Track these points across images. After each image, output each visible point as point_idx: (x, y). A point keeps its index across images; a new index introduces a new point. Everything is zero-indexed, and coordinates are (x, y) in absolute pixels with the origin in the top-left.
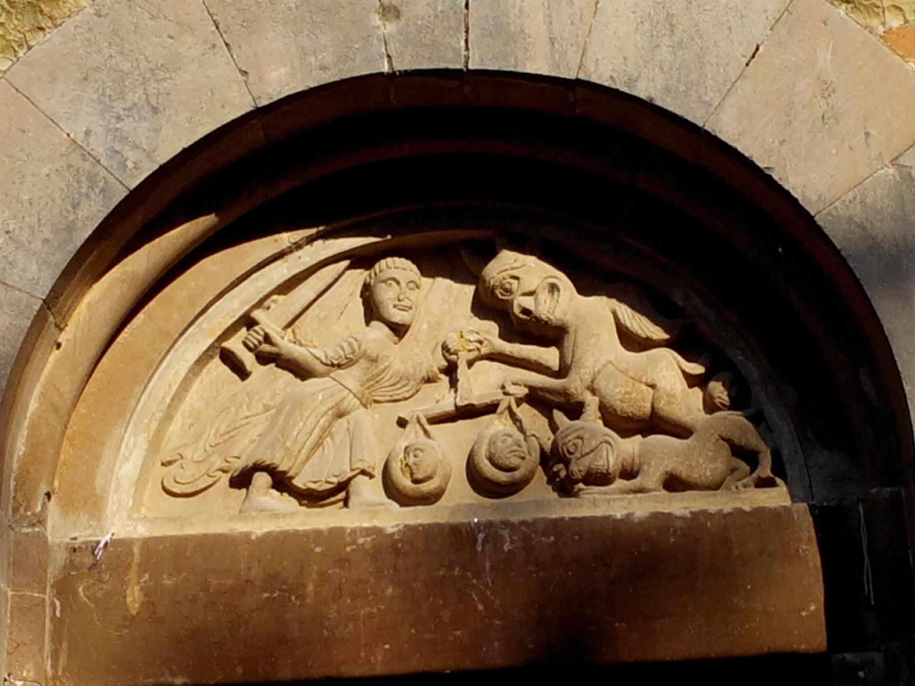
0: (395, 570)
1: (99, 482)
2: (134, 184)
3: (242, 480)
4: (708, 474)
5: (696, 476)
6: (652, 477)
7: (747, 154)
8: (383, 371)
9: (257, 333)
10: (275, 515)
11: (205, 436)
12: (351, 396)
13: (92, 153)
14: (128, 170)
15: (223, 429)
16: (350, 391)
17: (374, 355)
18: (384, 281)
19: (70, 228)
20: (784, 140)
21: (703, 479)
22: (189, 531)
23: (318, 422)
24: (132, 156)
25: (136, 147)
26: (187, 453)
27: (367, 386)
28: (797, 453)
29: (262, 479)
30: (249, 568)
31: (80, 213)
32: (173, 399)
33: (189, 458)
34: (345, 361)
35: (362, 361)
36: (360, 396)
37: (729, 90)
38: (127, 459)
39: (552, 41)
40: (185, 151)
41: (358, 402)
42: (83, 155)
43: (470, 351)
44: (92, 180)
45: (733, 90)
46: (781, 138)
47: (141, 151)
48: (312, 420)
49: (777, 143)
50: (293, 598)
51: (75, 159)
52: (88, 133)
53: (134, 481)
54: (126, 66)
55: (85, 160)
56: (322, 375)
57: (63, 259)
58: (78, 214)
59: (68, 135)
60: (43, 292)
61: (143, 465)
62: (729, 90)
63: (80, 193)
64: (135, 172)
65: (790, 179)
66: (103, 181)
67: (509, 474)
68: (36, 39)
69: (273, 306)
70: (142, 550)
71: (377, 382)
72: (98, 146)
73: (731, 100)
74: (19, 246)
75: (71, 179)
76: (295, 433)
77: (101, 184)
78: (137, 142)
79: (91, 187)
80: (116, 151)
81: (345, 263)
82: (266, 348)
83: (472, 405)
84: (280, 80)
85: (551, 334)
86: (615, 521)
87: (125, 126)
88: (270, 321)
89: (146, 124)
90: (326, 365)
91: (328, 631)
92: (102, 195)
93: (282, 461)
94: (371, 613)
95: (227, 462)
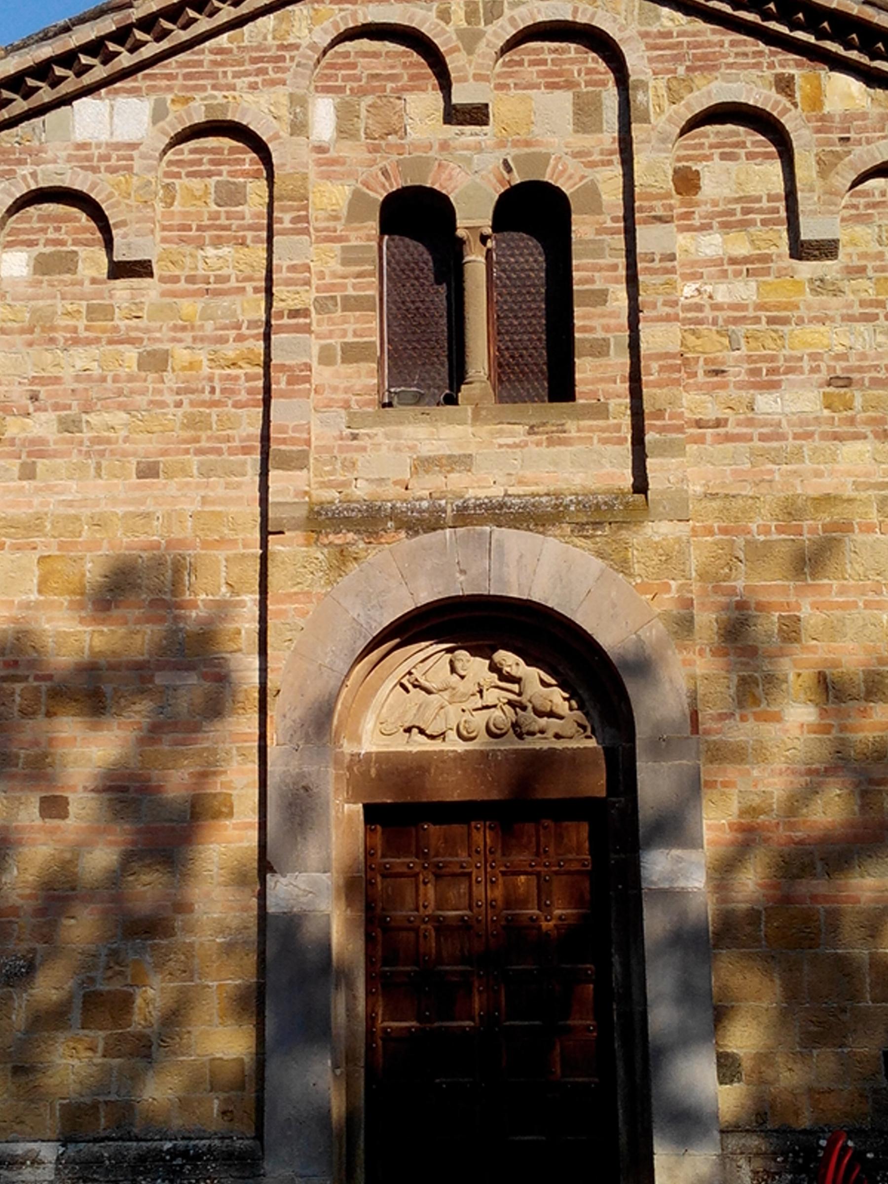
3: (408, 730)
6: (550, 734)
10: (420, 744)
19: (353, 650)
24: (374, 625)
29: (415, 731)
51: (354, 625)
88: (417, 674)
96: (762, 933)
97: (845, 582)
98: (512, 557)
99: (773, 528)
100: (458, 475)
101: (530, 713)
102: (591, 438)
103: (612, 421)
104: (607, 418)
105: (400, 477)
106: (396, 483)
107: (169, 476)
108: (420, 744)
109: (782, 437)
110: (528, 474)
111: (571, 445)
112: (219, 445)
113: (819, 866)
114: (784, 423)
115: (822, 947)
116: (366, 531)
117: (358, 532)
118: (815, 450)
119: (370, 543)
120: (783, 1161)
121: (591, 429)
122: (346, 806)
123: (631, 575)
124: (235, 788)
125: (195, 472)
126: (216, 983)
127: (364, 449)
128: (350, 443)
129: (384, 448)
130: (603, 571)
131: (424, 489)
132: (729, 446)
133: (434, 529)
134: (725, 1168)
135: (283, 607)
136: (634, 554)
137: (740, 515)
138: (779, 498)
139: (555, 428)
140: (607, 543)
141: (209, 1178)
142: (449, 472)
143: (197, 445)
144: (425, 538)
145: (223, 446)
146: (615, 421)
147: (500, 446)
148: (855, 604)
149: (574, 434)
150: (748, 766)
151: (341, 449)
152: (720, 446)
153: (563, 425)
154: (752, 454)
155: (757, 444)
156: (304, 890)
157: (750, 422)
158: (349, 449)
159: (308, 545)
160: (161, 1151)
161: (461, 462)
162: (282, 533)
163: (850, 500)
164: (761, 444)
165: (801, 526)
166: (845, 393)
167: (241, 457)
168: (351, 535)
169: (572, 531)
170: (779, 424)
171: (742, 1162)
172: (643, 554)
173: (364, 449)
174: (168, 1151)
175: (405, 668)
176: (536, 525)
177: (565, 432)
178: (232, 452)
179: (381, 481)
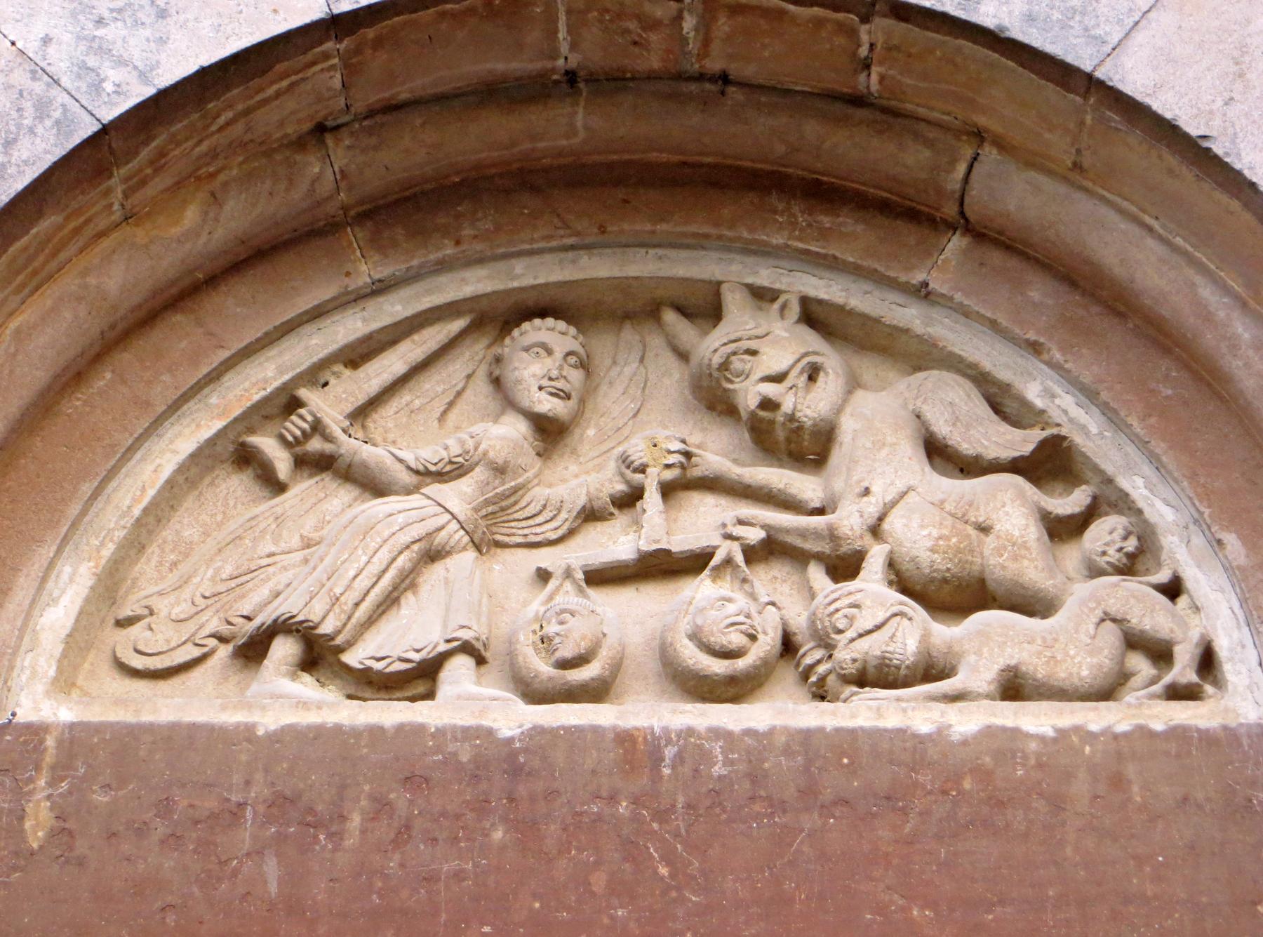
0: (511, 800)
2: (109, 115)
3: (253, 650)
4: (1085, 673)
5: (1063, 675)
6: (978, 673)
7: (1168, 115)
8: (515, 490)
9: (301, 417)
11: (196, 580)
12: (454, 525)
13: (48, 69)
14: (104, 95)
15: (228, 570)
16: (454, 517)
17: (500, 461)
18: (527, 349)
20: (1232, 99)
21: (1076, 681)
22: (146, 718)
23: (394, 559)
24: (113, 75)
27: (484, 512)
28: (1243, 647)
29: (284, 650)
30: (248, 783)
31: (16, 154)
32: (146, 511)
33: (163, 613)
34: (448, 468)
35: (478, 469)
36: (470, 527)
37: (1137, 23)
38: (55, 601)
40: (203, 72)
41: (466, 539)
42: (33, 72)
43: (668, 466)
44: (42, 108)
45: (1143, 22)
46: (1227, 95)
47: (129, 69)
48: (384, 556)
49: (1219, 103)
50: (322, 837)
51: (20, 77)
52: (47, 40)
53: (63, 636)
55: (34, 79)
56: (408, 491)
58: (11, 155)
59: (13, 44)
61: (80, 613)
62: (1137, 23)
63: (19, 126)
64: (114, 98)
65: (1243, 154)
66: (60, 110)
67: (726, 662)
69: (333, 381)
70: (60, 743)
71: (503, 509)
72: (60, 60)
73: (1139, 37)
75: (8, 105)
76: (352, 573)
77: (57, 114)
78: (126, 56)
79: (40, 118)
80: (88, 68)
81: (458, 325)
82: (315, 445)
83: (667, 552)
85: (810, 447)
86: (915, 736)
87: (112, 32)
88: (329, 405)
89: (147, 32)
90: (417, 472)
91: (381, 897)
92: (54, 131)
93: (324, 618)
94: (463, 871)
95: (229, 623)
101: (872, 582)
108: (304, 705)
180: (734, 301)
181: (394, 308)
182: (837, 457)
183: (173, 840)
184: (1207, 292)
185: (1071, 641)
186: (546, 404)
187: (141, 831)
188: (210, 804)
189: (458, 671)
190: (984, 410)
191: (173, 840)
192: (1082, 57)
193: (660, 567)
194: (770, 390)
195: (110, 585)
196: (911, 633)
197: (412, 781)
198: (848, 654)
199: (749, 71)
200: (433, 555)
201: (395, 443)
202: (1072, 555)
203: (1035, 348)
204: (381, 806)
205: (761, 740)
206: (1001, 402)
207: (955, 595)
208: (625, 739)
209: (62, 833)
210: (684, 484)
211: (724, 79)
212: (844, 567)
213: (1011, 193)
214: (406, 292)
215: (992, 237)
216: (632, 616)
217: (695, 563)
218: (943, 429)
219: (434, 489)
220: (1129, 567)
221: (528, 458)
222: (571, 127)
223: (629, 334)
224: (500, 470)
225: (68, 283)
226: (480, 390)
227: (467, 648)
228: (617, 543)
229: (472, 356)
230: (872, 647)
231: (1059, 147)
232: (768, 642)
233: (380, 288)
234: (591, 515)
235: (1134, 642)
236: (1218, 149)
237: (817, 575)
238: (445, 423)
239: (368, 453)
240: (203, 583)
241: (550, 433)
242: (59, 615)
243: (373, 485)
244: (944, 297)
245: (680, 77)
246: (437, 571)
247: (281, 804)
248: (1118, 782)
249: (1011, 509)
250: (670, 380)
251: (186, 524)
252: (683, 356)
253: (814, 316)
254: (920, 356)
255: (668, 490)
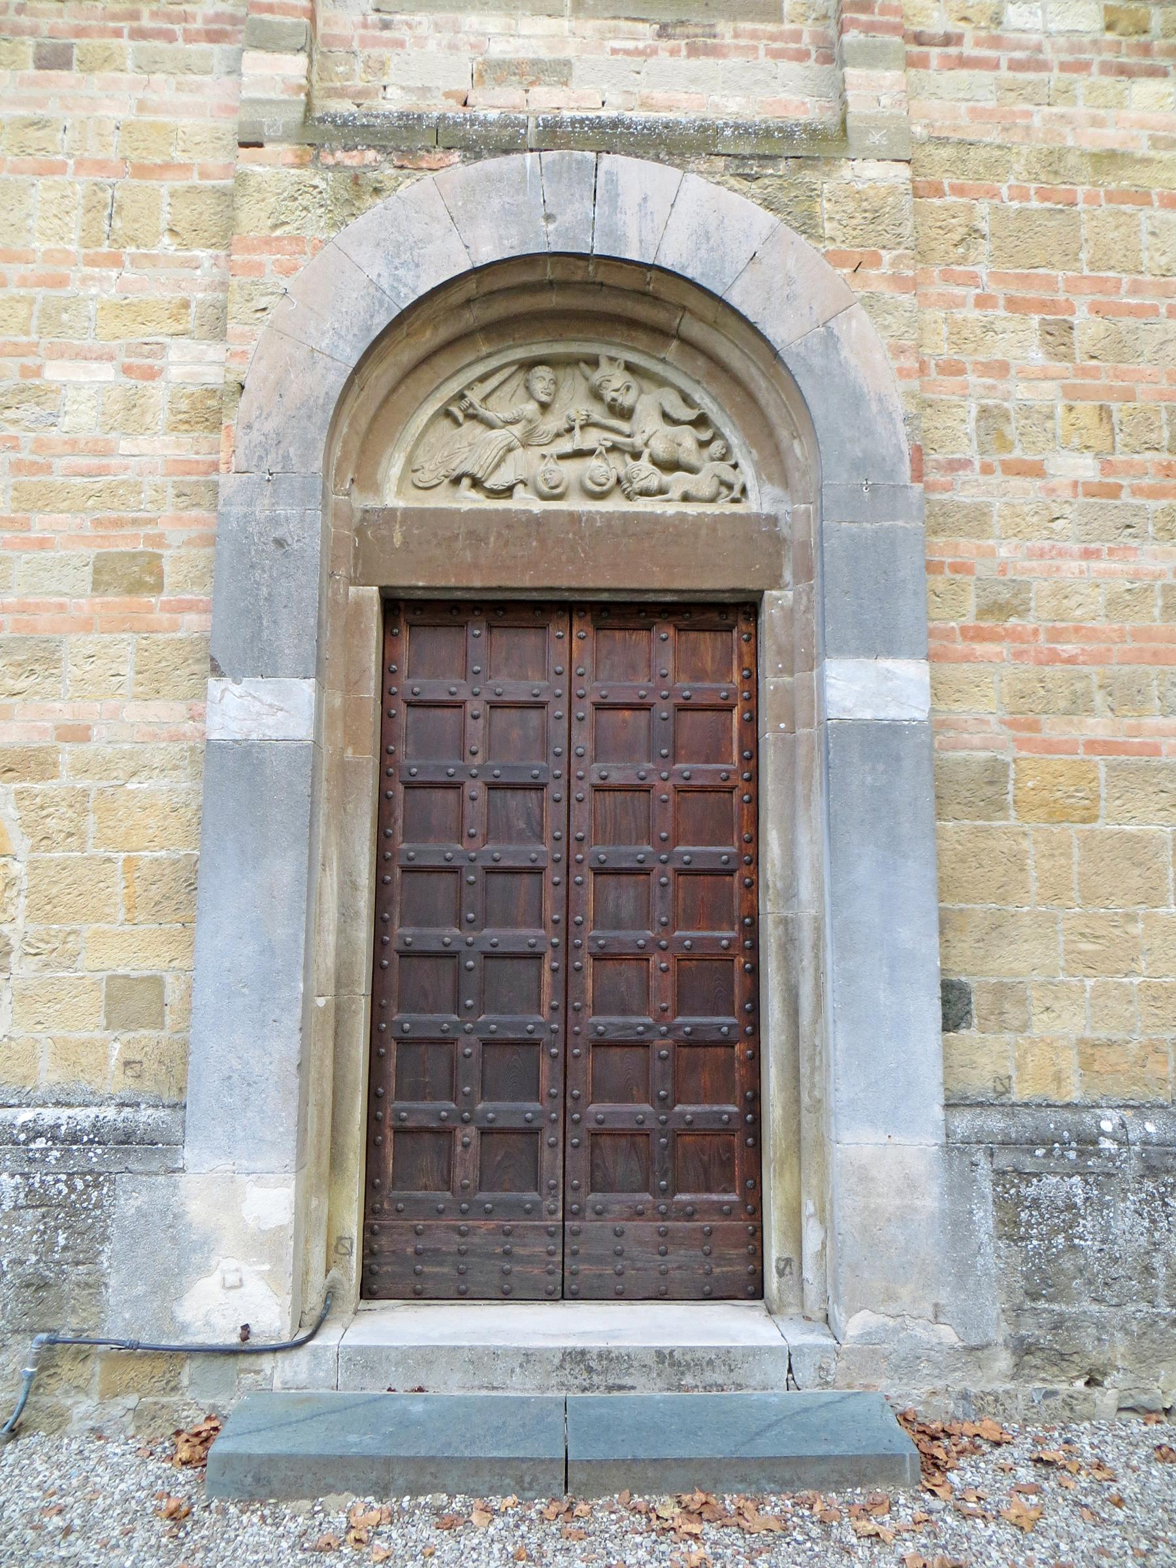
1: (379, 476)
2: (404, 306)
3: (456, 481)
6: (675, 493)
10: (474, 501)
19: (369, 329)
24: (404, 291)
25: (405, 285)
26: (426, 466)
29: (466, 482)
39: (641, 241)
51: (372, 290)
54: (401, 239)
57: (364, 346)
60: (353, 363)
68: (351, 221)
72: (385, 283)
74: (340, 337)
81: (514, 368)
82: (471, 411)
84: (488, 253)
85: (626, 414)
87: (401, 272)
88: (474, 397)
96: (1010, 798)
97: (1140, 277)
98: (629, 200)
99: (1032, 192)
100: (546, 89)
101: (644, 461)
102: (755, 48)
103: (787, 26)
104: (781, 20)
105: (455, 88)
106: (448, 95)
107: (89, 68)
108: (474, 501)
109: (1042, 66)
110: (659, 95)
111: (724, 56)
112: (170, 26)
113: (1099, 698)
114: (1047, 47)
115: (1100, 821)
116: (397, 149)
117: (382, 149)
118: (1091, 89)
119: (402, 167)
120: (1045, 1156)
121: (754, 35)
122: (352, 589)
123: (820, 238)
124: (169, 546)
125: (129, 64)
126: (123, 855)
127: (401, 44)
128: (378, 33)
129: (432, 45)
130: (774, 231)
131: (493, 104)
132: (964, 73)
133: (507, 152)
134: (951, 1166)
135: (257, 258)
136: (824, 207)
137: (981, 170)
138: (1040, 152)
139: (699, 31)
140: (781, 188)
141: (91, 1172)
142: (532, 83)
143: (135, 24)
144: (492, 165)
145: (176, 27)
146: (793, 26)
147: (614, 51)
148: (1155, 310)
149: (728, 40)
150: (991, 542)
151: (364, 42)
152: (952, 73)
153: (711, 26)
154: (999, 88)
155: (1004, 73)
156: (271, 706)
157: (996, 42)
158: (376, 42)
159: (301, 166)
160: (12, 1125)
161: (558, 71)
162: (260, 145)
163: (1146, 161)
164: (1010, 74)
165: (1075, 192)
166: (1137, 10)
167: (205, 46)
168: (371, 155)
169: (726, 167)
170: (1039, 49)
171: (980, 1157)
172: (838, 208)
173: (401, 44)
174: (24, 1127)
175: (453, 387)
176: (670, 154)
177: (715, 37)
178: (189, 38)
179: (425, 90)
180: (603, 362)
181: (494, 363)
182: (635, 417)
183: (439, 544)
184: (753, 370)
185: (702, 483)
186: (544, 398)
187: (429, 542)
188: (448, 534)
189: (520, 488)
190: (681, 403)
191: (439, 544)
192: (719, 291)
193: (579, 454)
194: (614, 394)
195: (410, 460)
196: (656, 478)
197: (508, 527)
198: (637, 486)
199: (610, 282)
200: (510, 450)
201: (497, 411)
202: (706, 453)
203: (698, 382)
204: (500, 534)
205: (609, 517)
206: (686, 399)
207: (670, 466)
208: (571, 514)
209: (405, 543)
210: (588, 425)
211: (602, 284)
212: (636, 456)
213: (694, 330)
214: (785, 1119)
215: (687, 343)
216: (571, 469)
217: (591, 453)
218: (668, 409)
219: (510, 427)
220: (723, 458)
221: (538, 416)
222: (553, 300)
223: (569, 370)
224: (530, 421)
225: (390, 360)
226: (521, 391)
227: (522, 482)
228: (566, 445)
229: (519, 378)
230: (644, 484)
231: (710, 315)
232: (613, 480)
233: (489, 355)
234: (558, 435)
235: (723, 483)
236: (759, 327)
237: (628, 458)
238: (509, 404)
239: (489, 414)
240: (438, 458)
241: (544, 407)
242: (396, 471)
243: (491, 426)
244: (669, 363)
245: (587, 283)
246: (512, 455)
247: (471, 534)
248: (714, 530)
249: (688, 438)
250: (582, 387)
251: (431, 438)
252: (587, 379)
253: (630, 368)
254: (662, 382)
255: (582, 427)
